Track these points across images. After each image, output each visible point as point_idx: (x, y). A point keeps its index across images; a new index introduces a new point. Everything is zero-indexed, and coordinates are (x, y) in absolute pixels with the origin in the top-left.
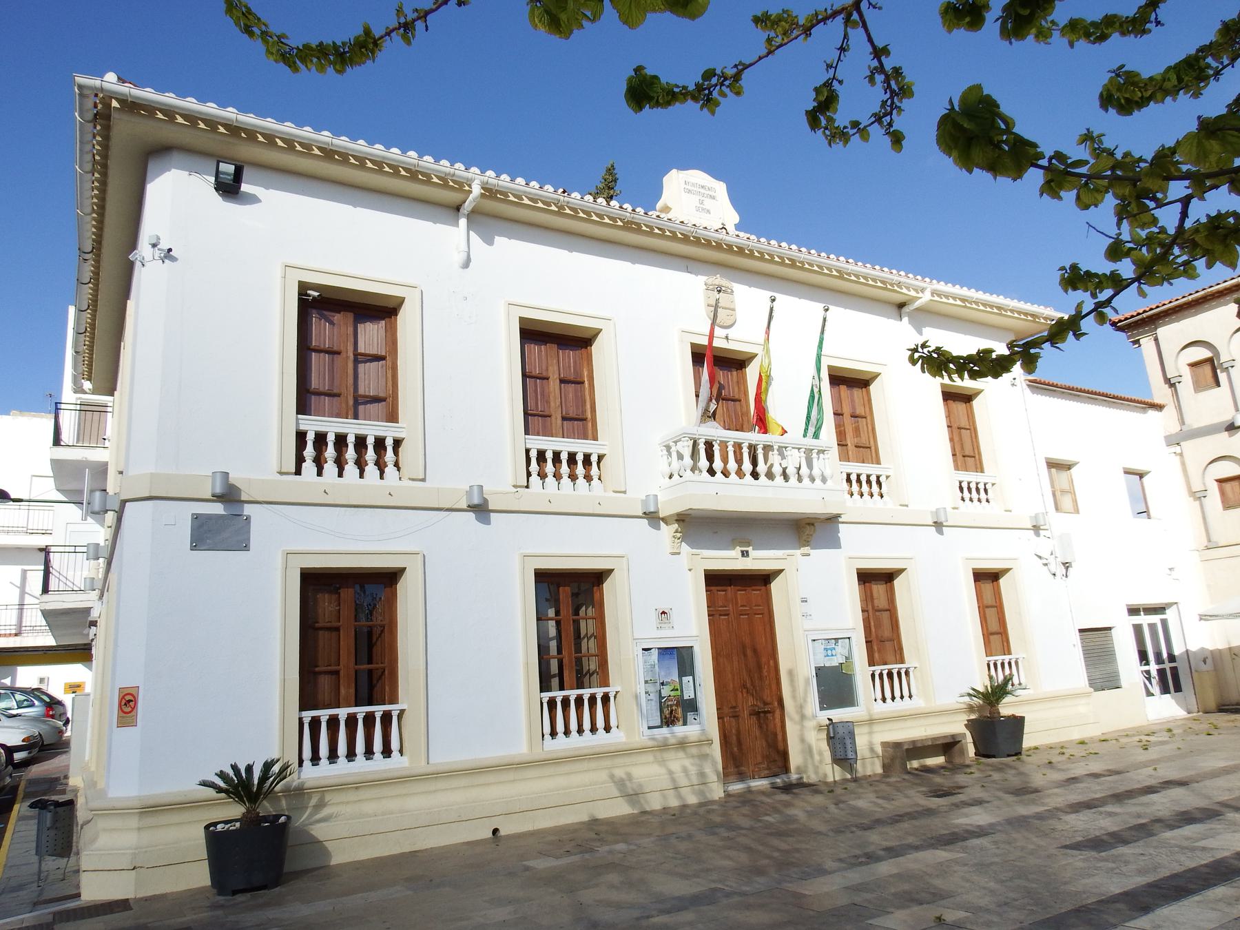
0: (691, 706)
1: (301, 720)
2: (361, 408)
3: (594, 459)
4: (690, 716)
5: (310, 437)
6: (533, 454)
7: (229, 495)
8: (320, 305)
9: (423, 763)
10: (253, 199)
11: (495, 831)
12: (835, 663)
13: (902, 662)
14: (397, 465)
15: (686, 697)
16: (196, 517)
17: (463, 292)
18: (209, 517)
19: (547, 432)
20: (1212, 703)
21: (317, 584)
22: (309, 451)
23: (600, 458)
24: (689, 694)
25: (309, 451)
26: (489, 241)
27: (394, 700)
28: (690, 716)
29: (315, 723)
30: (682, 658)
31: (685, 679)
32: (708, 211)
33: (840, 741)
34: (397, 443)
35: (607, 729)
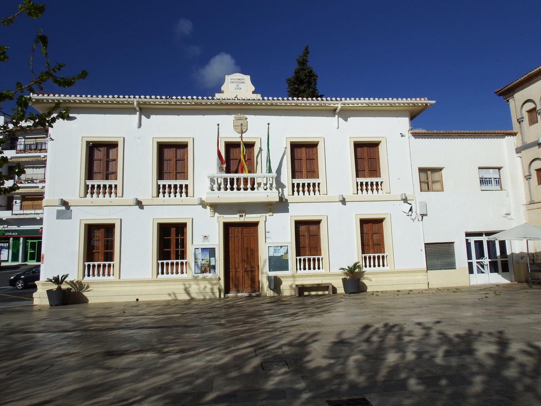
0: (214, 267)
1: (297, 259)
2: (178, 175)
3: (379, 183)
4: (212, 271)
5: (296, 185)
6: (359, 183)
7: (65, 203)
8: (92, 148)
9: (393, 269)
10: (74, 118)
11: (137, 300)
12: (279, 255)
13: (384, 253)
14: (319, 191)
15: (212, 264)
16: (58, 211)
17: (137, 135)
18: (61, 210)
19: (364, 177)
20: (523, 278)
21: (91, 230)
22: (296, 189)
23: (382, 183)
24: (212, 263)
25: (296, 189)
26: (148, 117)
27: (320, 255)
28: (212, 271)
29: (365, 258)
30: (212, 252)
31: (212, 259)
32: (241, 89)
33: (276, 284)
34: (319, 184)
35: (383, 266)
